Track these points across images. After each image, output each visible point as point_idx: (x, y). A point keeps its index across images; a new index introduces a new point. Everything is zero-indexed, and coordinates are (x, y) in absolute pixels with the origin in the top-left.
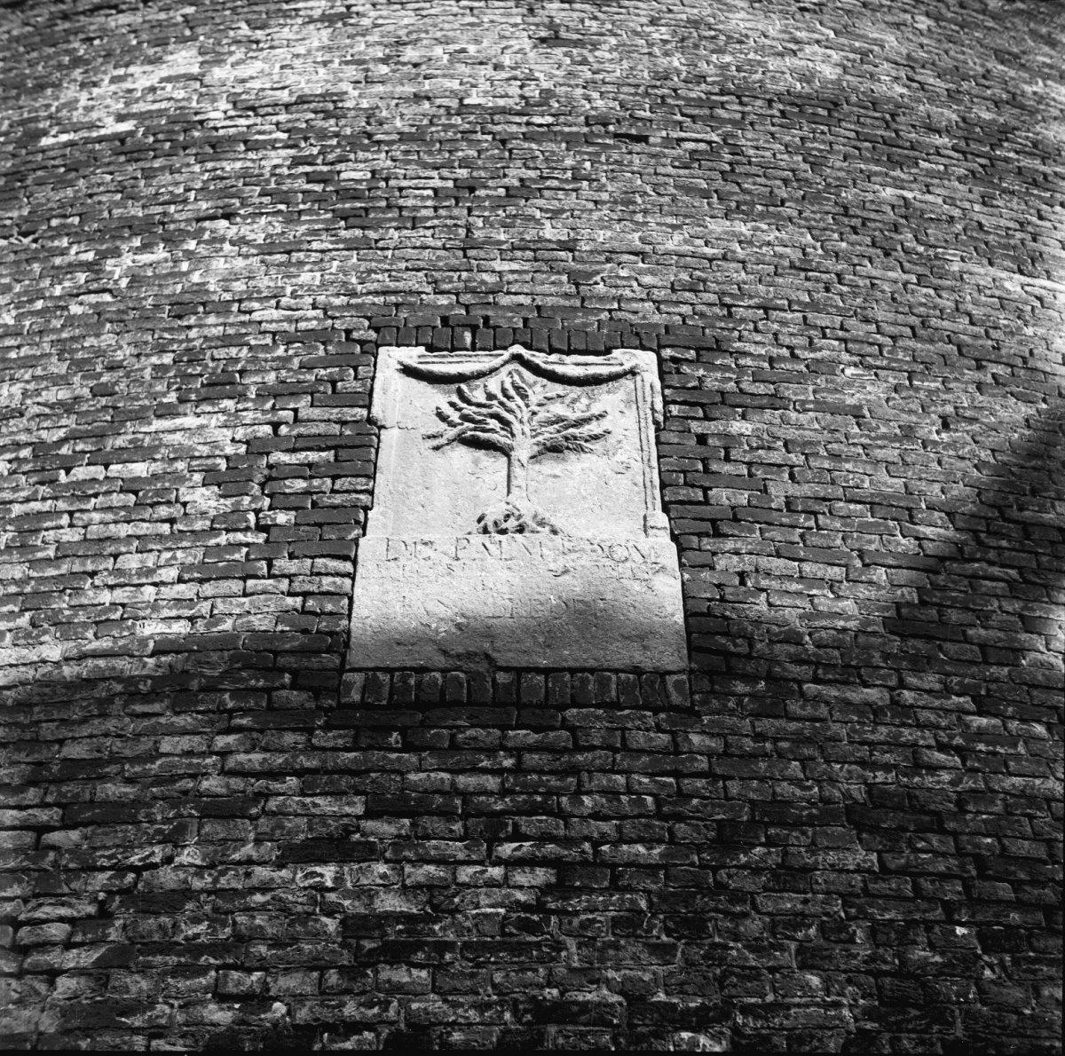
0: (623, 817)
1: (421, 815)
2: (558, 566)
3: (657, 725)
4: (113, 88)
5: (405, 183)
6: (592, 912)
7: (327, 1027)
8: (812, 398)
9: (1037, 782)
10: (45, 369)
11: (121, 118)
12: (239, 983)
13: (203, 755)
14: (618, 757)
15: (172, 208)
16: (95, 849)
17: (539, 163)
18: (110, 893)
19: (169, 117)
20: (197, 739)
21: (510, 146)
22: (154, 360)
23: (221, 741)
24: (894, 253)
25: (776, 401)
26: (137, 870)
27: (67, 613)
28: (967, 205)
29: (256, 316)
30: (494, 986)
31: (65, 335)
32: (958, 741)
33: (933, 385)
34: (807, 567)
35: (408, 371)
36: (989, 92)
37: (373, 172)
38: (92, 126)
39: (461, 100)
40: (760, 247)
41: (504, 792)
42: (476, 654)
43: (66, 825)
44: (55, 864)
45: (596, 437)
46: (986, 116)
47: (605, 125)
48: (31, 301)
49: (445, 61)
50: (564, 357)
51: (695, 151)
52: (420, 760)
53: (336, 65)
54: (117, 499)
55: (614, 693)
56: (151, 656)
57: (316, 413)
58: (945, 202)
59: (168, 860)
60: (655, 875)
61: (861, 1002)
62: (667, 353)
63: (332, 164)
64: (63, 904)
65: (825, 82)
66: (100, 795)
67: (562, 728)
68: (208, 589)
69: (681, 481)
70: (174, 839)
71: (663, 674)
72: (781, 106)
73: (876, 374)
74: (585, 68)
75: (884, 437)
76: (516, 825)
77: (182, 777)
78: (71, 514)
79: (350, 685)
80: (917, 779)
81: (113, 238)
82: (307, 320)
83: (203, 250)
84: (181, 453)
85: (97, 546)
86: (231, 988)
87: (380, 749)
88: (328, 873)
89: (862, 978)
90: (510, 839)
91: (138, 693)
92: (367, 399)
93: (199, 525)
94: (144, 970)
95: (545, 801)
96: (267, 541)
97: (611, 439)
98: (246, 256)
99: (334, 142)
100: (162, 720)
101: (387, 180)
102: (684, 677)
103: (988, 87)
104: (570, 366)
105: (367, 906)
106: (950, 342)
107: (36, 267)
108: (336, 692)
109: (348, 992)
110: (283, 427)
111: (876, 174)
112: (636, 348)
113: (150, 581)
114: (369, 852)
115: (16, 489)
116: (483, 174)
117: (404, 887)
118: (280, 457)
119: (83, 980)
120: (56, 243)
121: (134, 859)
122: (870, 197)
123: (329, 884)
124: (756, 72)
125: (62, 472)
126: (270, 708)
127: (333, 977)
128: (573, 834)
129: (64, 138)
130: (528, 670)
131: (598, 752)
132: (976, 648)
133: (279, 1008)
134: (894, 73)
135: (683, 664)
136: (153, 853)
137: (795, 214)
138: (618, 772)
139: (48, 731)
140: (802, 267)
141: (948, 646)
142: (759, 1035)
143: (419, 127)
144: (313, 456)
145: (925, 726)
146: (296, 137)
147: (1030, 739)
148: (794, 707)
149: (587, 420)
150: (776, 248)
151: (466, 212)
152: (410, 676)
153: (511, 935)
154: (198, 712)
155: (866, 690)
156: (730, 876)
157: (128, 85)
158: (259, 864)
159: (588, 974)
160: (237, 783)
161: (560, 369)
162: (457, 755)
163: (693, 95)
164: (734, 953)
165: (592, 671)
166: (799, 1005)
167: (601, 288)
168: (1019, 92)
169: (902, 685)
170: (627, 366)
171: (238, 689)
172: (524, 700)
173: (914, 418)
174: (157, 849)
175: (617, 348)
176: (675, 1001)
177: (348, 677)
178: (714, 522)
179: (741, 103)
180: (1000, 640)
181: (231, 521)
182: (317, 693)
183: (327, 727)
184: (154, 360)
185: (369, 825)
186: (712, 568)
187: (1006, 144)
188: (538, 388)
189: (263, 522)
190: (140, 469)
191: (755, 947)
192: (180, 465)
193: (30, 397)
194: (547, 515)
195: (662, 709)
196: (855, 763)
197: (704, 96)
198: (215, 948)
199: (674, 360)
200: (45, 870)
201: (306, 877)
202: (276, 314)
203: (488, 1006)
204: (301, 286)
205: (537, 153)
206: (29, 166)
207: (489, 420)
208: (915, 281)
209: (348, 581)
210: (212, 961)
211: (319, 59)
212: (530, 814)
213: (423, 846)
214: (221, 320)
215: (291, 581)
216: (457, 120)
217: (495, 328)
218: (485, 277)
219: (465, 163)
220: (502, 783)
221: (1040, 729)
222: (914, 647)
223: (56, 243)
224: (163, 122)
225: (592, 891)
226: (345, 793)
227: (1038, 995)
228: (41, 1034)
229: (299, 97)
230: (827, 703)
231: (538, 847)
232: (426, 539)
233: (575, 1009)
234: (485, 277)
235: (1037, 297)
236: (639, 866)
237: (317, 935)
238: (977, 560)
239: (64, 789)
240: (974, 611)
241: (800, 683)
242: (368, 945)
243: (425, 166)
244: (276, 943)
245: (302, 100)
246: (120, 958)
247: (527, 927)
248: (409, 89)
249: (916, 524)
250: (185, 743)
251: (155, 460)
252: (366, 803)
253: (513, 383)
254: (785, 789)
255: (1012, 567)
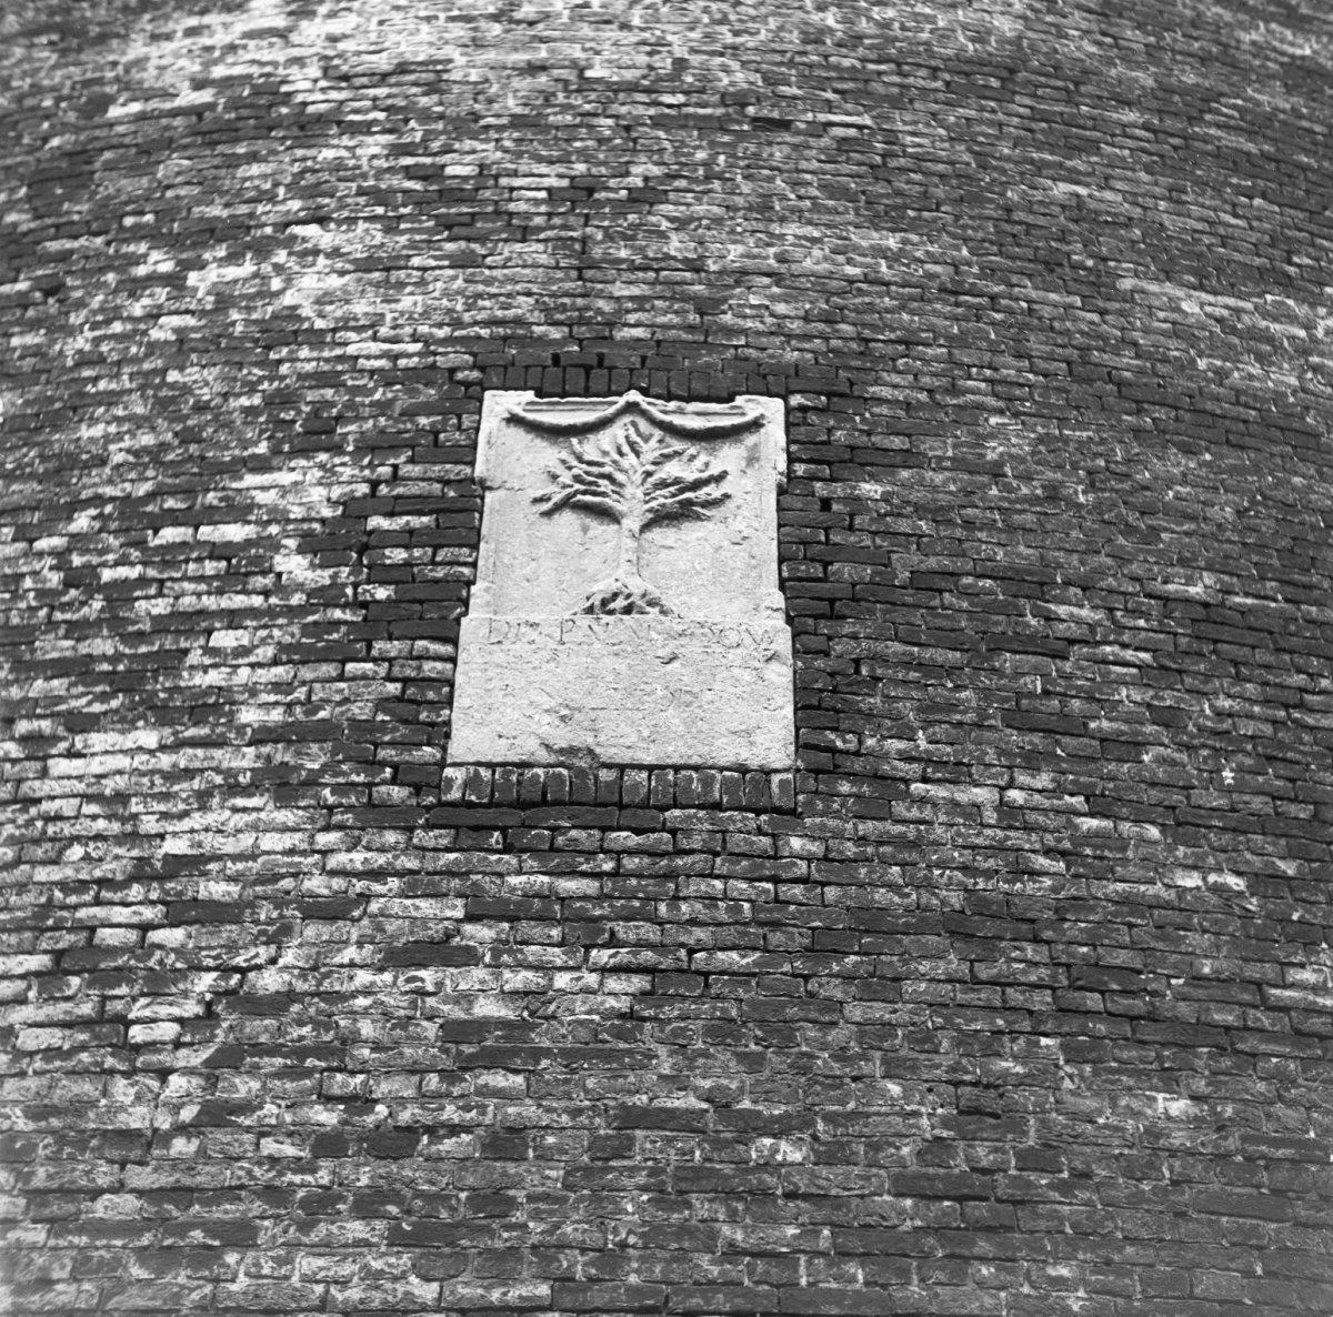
0: (720, 924)
1: (518, 919)
2: (665, 653)
3: (759, 827)
4: (188, 41)
5: (517, 182)
6: (683, 1019)
7: (430, 1130)
8: (950, 454)
9: (1143, 888)
10: (126, 408)
11: (198, 85)
12: (345, 1085)
13: (303, 853)
14: (718, 860)
15: (260, 209)
16: (201, 949)
17: (667, 158)
18: (216, 993)
19: (253, 86)
20: (299, 835)
21: (634, 135)
22: (244, 401)
23: (324, 839)
24: (1059, 270)
25: (910, 458)
26: (243, 971)
27: (162, 695)
28: (1150, 202)
29: (351, 350)
30: (587, 1092)
31: (146, 366)
32: (1067, 845)
33: (1085, 434)
34: (928, 654)
35: (514, 420)
36: (1196, 45)
37: (481, 166)
38: (167, 94)
39: (582, 71)
40: (908, 266)
41: (602, 897)
42: (579, 749)
43: (172, 922)
44: (161, 962)
45: (707, 504)
46: (1190, 79)
47: (744, 105)
48: (108, 322)
49: (565, 19)
50: (683, 404)
51: (845, 139)
52: (520, 862)
53: (441, 22)
54: (210, 567)
55: (717, 795)
56: (249, 745)
57: (417, 470)
58: (1125, 200)
59: (273, 961)
60: (747, 983)
61: (940, 1111)
62: (796, 400)
63: (435, 154)
64: (171, 1004)
65: (1002, 41)
66: (202, 895)
67: (663, 830)
68: (307, 673)
69: (801, 555)
70: (278, 937)
71: (767, 772)
72: (947, 77)
73: (1023, 423)
74: (724, 29)
75: (1025, 500)
76: (613, 933)
77: (283, 876)
78: (161, 582)
79: (450, 781)
80: (1019, 885)
81: (194, 245)
82: (410, 356)
83: (292, 264)
84: (278, 516)
85: (194, 623)
86: (336, 1091)
87: (481, 850)
88: (428, 976)
89: (942, 1088)
90: (605, 946)
91: (238, 784)
92: (467, 454)
93: (297, 599)
94: (253, 1071)
95: (643, 907)
96: (365, 619)
97: (730, 505)
98: (342, 273)
99: (440, 126)
100: (263, 815)
101: (496, 177)
102: (790, 776)
103: (1196, 39)
104: (692, 417)
105: (468, 1011)
106: (1111, 381)
107: (111, 277)
108: (440, 785)
109: (448, 1095)
110: (382, 487)
111: (1048, 165)
112: (762, 394)
113: (246, 661)
114: (469, 957)
115: (102, 552)
116: (603, 170)
117: (503, 992)
118: (376, 522)
119: (196, 1081)
120: (132, 248)
121: (240, 961)
122: (1038, 195)
123: (430, 988)
124: (922, 30)
125: (150, 532)
126: (371, 804)
127: (433, 1081)
128: (667, 941)
129: (135, 107)
130: (633, 767)
131: (697, 857)
132: (1095, 743)
133: (381, 1109)
134: (1084, 25)
135: (788, 762)
136: (257, 955)
137: (949, 218)
138: (718, 877)
139: (149, 825)
140: (952, 291)
141: (1066, 740)
142: (838, 1142)
143: (534, 107)
144: (416, 522)
145: (1032, 830)
146: (398, 118)
147: (1143, 841)
148: (899, 808)
149: (706, 482)
150: (927, 266)
151: (582, 221)
152: (512, 772)
153: (604, 1042)
154: (298, 808)
155: (976, 790)
156: (821, 985)
157: (205, 41)
158: (362, 967)
159: (677, 1082)
160: (338, 883)
161: (677, 420)
162: (559, 858)
163: (847, 63)
164: (819, 1062)
165: (696, 768)
166: (878, 1114)
167: (728, 318)
168: (1233, 43)
169: (1011, 785)
170: (750, 417)
171: (339, 784)
172: (626, 800)
173: (1059, 476)
174: (262, 950)
175: (741, 394)
176: (761, 1108)
177: (449, 772)
178: (832, 602)
179: (900, 74)
180: (1123, 733)
181: (326, 596)
182: (418, 790)
183: (429, 826)
184: (244, 401)
185: (468, 928)
186: (827, 654)
187: (1208, 117)
188: (653, 443)
189: (361, 598)
190: (235, 532)
191: (841, 1055)
192: (274, 529)
193: (112, 442)
194: (657, 593)
195: (765, 811)
196: (957, 868)
197: (858, 65)
198: (320, 1051)
199: (803, 409)
200: (151, 969)
201: (408, 981)
202: (375, 348)
203: (578, 1112)
204: (402, 313)
205: (666, 144)
206: (98, 144)
207: (600, 481)
208: (1079, 304)
209: (449, 666)
210: (317, 1063)
211: (422, 14)
212: (627, 919)
213: (521, 951)
214: (315, 354)
215: (391, 666)
216: (577, 101)
217: (610, 369)
218: (601, 303)
219: (584, 155)
220: (602, 887)
221: (1153, 832)
222: (1030, 743)
223: (132, 248)
224: (246, 93)
225: (684, 998)
226: (446, 895)
227: (1114, 1105)
228: (156, 1130)
229: (399, 65)
230: (935, 805)
231: (635, 954)
232: (533, 618)
233: (663, 1116)
234: (601, 303)
235: (1217, 320)
236: (734, 974)
237: (417, 1040)
238: (1110, 643)
239: (169, 885)
240: (1099, 700)
241: (907, 782)
242: (467, 1049)
243: (540, 159)
244: (377, 1047)
245: (403, 68)
246: (231, 1058)
247: (619, 1035)
248: (521, 57)
249: (1048, 601)
250: (289, 840)
251: (249, 522)
252: (466, 905)
253: (627, 437)
254: (881, 896)
255: (1146, 650)
